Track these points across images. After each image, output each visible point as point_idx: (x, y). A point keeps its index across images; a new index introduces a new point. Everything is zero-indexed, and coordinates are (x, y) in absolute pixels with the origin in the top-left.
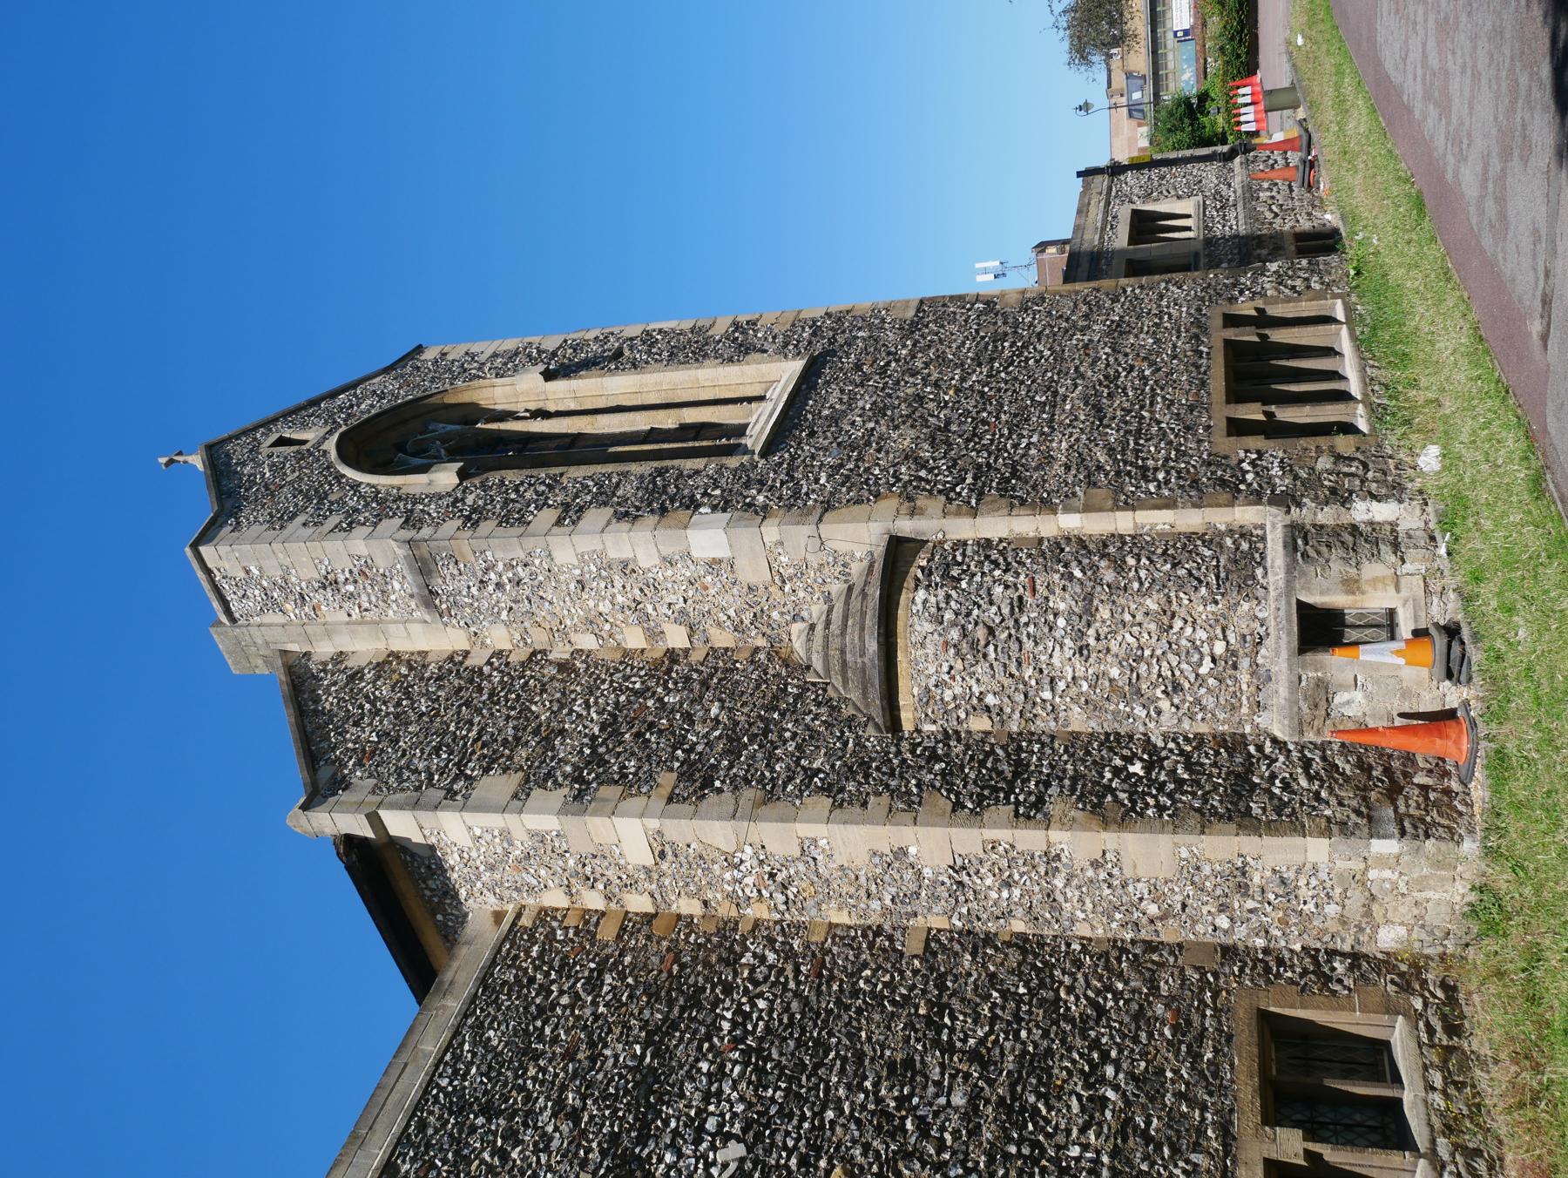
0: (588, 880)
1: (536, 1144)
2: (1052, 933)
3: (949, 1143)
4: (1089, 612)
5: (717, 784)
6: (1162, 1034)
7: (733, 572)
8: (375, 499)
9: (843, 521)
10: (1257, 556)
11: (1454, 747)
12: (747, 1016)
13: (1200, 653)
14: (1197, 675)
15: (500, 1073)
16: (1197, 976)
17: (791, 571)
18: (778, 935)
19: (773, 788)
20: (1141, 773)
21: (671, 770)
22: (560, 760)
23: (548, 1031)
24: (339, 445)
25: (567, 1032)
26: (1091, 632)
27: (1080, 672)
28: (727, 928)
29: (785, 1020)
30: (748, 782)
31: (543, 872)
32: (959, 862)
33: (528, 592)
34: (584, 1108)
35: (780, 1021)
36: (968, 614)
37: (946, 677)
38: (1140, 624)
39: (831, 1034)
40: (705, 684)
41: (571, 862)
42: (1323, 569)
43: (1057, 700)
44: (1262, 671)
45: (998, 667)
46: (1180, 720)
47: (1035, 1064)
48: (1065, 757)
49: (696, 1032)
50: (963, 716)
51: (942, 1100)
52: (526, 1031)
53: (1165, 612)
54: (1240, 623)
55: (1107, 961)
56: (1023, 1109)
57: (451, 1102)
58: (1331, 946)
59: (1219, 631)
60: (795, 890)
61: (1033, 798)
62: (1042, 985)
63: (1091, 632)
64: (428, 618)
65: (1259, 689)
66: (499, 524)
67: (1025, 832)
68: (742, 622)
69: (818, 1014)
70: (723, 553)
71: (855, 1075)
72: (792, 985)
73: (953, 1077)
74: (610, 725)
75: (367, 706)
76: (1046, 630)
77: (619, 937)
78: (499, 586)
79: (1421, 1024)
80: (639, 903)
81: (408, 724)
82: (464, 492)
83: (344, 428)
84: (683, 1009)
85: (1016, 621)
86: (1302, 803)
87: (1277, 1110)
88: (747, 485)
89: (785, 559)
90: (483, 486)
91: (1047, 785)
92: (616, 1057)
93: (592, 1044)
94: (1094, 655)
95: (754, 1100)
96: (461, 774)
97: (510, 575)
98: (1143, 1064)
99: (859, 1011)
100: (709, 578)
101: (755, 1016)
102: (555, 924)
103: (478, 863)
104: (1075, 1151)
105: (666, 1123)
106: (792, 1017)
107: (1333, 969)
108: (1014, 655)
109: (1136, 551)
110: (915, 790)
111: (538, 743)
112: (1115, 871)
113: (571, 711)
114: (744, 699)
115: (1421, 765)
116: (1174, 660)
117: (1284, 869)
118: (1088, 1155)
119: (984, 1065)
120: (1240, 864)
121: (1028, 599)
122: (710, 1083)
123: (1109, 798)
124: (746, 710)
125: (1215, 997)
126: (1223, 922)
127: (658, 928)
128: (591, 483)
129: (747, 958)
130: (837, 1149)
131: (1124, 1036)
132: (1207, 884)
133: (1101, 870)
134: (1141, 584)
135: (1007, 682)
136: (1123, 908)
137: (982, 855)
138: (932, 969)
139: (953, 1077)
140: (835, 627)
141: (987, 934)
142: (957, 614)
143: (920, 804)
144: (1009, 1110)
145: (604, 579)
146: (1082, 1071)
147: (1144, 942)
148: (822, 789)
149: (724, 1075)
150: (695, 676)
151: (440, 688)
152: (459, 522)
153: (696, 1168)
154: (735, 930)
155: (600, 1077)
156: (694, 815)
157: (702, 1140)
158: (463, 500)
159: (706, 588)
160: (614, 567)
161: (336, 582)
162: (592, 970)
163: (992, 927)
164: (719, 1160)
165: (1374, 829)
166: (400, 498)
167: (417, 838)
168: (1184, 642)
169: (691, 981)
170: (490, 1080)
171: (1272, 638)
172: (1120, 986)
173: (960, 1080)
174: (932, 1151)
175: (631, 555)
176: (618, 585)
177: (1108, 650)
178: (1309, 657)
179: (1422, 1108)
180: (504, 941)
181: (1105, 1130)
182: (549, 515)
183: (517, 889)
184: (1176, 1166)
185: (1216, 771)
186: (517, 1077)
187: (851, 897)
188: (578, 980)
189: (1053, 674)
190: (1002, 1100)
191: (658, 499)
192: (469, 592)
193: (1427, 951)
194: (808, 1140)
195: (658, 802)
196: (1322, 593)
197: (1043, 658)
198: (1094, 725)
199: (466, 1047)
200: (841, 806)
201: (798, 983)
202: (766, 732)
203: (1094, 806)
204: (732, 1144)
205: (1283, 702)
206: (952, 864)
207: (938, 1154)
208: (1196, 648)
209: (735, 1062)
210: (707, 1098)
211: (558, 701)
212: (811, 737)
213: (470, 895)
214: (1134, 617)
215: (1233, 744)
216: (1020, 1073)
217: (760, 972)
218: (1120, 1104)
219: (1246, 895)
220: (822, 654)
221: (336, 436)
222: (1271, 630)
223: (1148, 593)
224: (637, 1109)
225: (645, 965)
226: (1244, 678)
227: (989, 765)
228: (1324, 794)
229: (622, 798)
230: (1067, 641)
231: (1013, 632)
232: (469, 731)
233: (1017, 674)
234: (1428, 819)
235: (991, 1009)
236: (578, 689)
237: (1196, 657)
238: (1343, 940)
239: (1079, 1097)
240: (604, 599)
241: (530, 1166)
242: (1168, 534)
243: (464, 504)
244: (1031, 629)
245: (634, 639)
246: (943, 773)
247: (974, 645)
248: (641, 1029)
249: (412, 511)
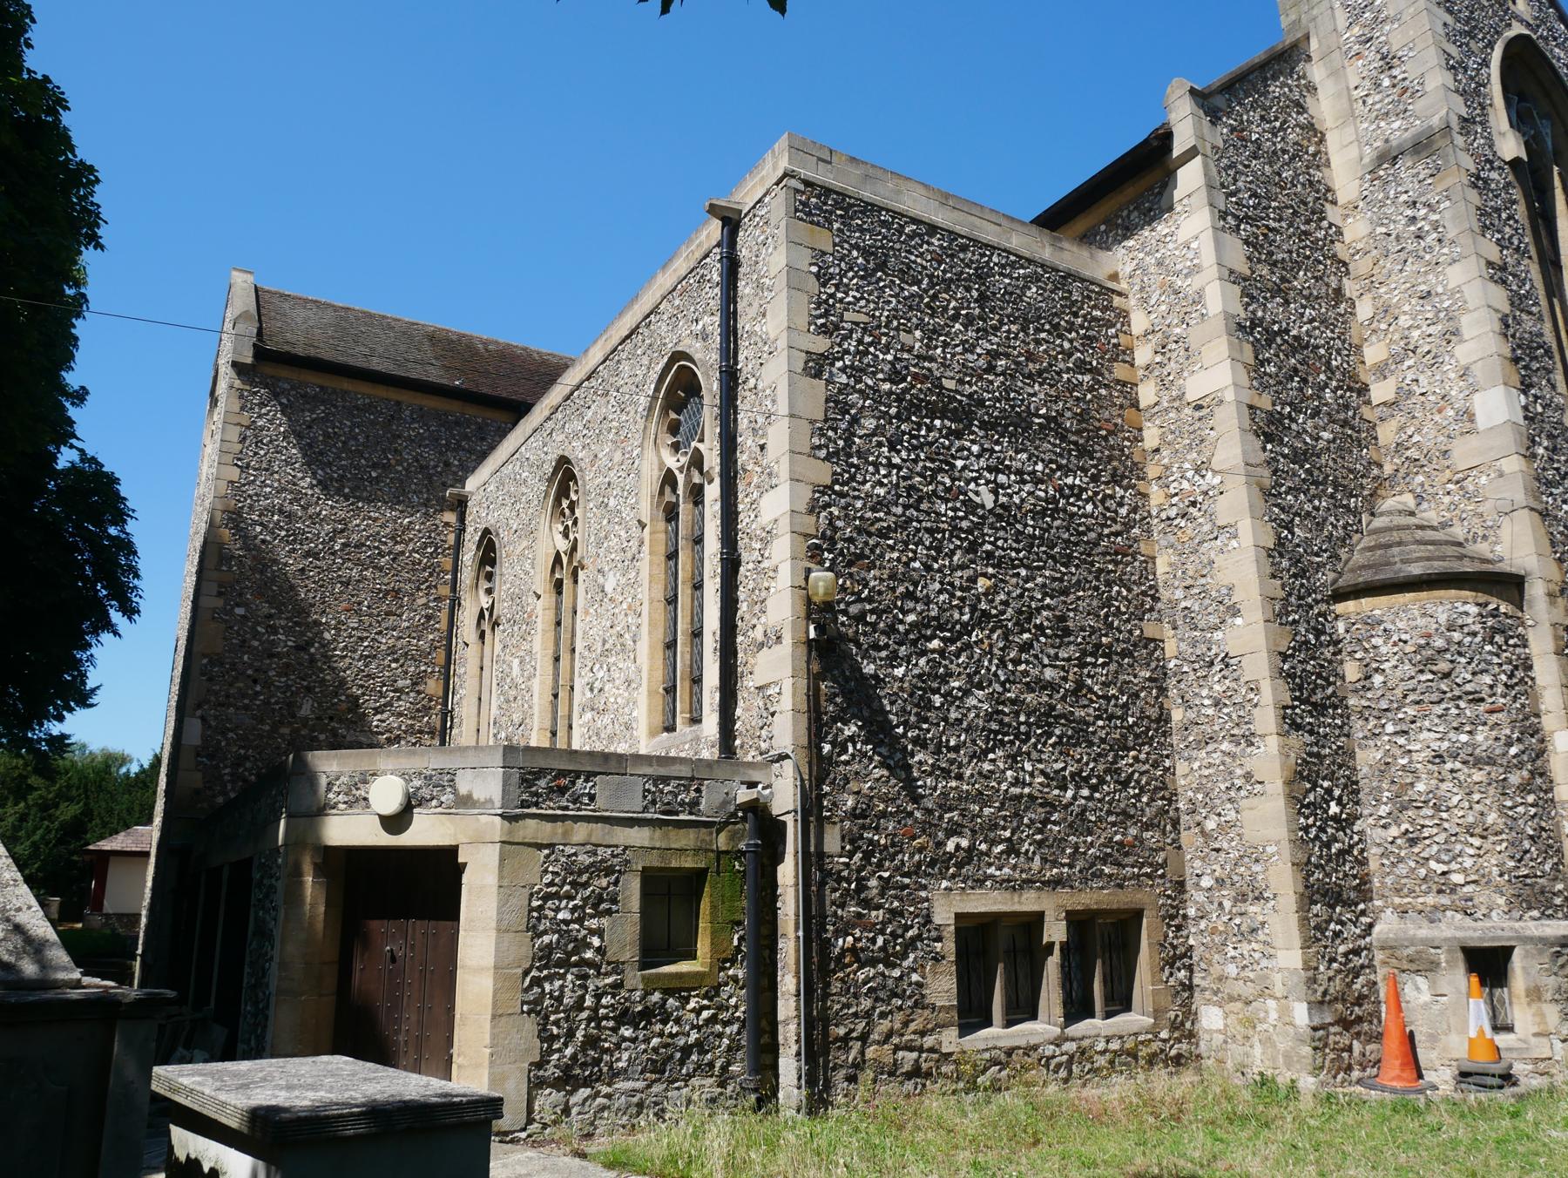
0: (1162, 349)
1: (967, 341)
2: (1175, 743)
3: (1019, 668)
4: (1478, 763)
5: (1269, 446)
6: (1116, 833)
7: (1462, 434)
8: (1479, 85)
9: (1534, 531)
10: (1550, 912)
11: (1393, 1073)
12: (1079, 497)
13: (1450, 862)
14: (1427, 859)
15: (1008, 302)
16: (1160, 861)
17: (1471, 488)
18: (1139, 516)
19: (1274, 495)
20: (1331, 812)
21: (1274, 405)
22: (1265, 305)
23: (1043, 335)
24: (1519, 37)
25: (1045, 351)
26: (1458, 765)
27: (1415, 756)
28: (1137, 470)
29: (1081, 529)
30: (1275, 472)
32: (1232, 661)
33: (1410, 247)
34: (997, 375)
35: (1079, 525)
36: (1460, 654)
37: (1395, 638)
38: (1471, 808)
39: (1077, 567)
40: (1345, 423)
41: (1178, 330)
42: (1547, 970)
43: (1386, 738)
44: (1439, 915)
45: (1411, 684)
46: (1379, 845)
47: (1080, 736)
48: (1334, 747)
49: (1061, 455)
50: (1358, 656)
51: (1046, 661)
52: (1040, 317)
53: (1486, 830)
54: (1482, 896)
55: (1161, 789)
56: (1049, 725)
57: (983, 268)
58: (1196, 968)
59: (1474, 877)
60: (1182, 524)
61: (1299, 721)
62: (1137, 736)
63: (1458, 765)
64: (1366, 160)
65: (1420, 912)
66: (1478, 209)
67: (1273, 714)
68: (1407, 449)
69: (1089, 555)
70: (1482, 422)
71: (1053, 590)
72: (1106, 531)
73: (1063, 668)
74: (1299, 344)
75: (1278, 124)
76: (1455, 724)
77: (1118, 382)
78: (1413, 220)
79: (1150, 1036)
80: (1147, 394)
81: (1271, 164)
82: (1500, 168)
83: (1535, 37)
84: (1075, 443)
85: (1460, 698)
86: (1326, 947)
87: (1078, 922)
88: (1550, 436)
89: (1484, 480)
90: (1508, 184)
91: (1311, 733)
92: (1034, 395)
93: (1040, 372)
94: (1435, 768)
95: (1023, 510)
96: (1240, 220)
97: (1427, 228)
98: (1093, 819)
99: (1096, 588)
100: (1451, 413)
101: (1080, 503)
102: (1119, 326)
103: (1163, 251)
104: (1028, 766)
105: (997, 443)
106: (1084, 533)
107: (1179, 970)
108: (1426, 698)
109: (1541, 803)
110: (1290, 619)
111: (1275, 283)
112: (1243, 793)
113: (1304, 307)
114: (1339, 460)
115: (1368, 1048)
116: (1441, 838)
117: (1267, 931)
118: (1027, 777)
119: (1075, 692)
120: (1266, 895)
121: (1482, 707)
122: (1029, 474)
123: (1308, 786)
124: (1331, 463)
125: (1147, 875)
126: (1206, 882)
127: (1129, 413)
128: (1527, 287)
129: (1119, 492)
130: (1002, 581)
131: (1110, 803)
132: (1242, 869)
133: (1243, 780)
134: (1511, 808)
135: (1398, 692)
136: (1208, 800)
137: (1243, 680)
138: (1135, 645)
139: (1063, 668)
140: (1419, 534)
141: (1166, 689)
142: (1459, 643)
143: (1281, 624)
144: (1048, 715)
145: (1436, 315)
146: (1082, 771)
147: (1179, 818)
148: (1279, 538)
149: (1036, 484)
150: (1350, 413)
151: (1303, 185)
152: (1473, 170)
153: (972, 471)
154: (1139, 478)
155: (1019, 384)
156: (1243, 430)
157: (990, 473)
158: (1492, 168)
159: (1440, 411)
160: (1451, 323)
161: (1390, 68)
162: (1090, 363)
163: (1173, 693)
164: (980, 488)
165: (1318, 1004)
166: (1483, 108)
167: (1178, 194)
168: (1458, 847)
169: (1097, 448)
170: (1003, 295)
171: (1474, 924)
172: (1145, 799)
173: (1062, 674)
174: (1012, 655)
175: (1466, 337)
176: (1431, 330)
177: (1442, 781)
178: (1460, 955)
179: (1093, 1033)
180: (1100, 286)
181: (1046, 790)
182: (1493, 253)
183: (1142, 289)
184: (1030, 844)
185: (1341, 876)
186: (1008, 317)
187: (1183, 573)
188: (1082, 353)
189: (1412, 733)
190: (1053, 708)
191: (1524, 353)
192: (1401, 193)
193: (1202, 1044)
194: (1004, 557)
195: (1248, 396)
196: (1524, 968)
197: (1427, 723)
198: (1364, 771)
199: (1022, 271)
200: (1269, 556)
201: (1108, 536)
202: (1316, 483)
203: (1300, 773)
204: (992, 497)
205: (1411, 933)
206: (1231, 655)
207: (1011, 660)
208: (1454, 858)
209: (1046, 492)
210: (1019, 472)
211: (1311, 294)
212: (1318, 524)
213: (1130, 249)
214: (1478, 802)
215: (1364, 891)
216: (1074, 721)
217: (1110, 503)
218: (1064, 802)
219: (1236, 901)
220: (1391, 525)
221: (1526, 32)
222: (1480, 924)
223: (1502, 814)
224: (1003, 418)
225: (1101, 407)
226: (1431, 899)
227: (1319, 681)
228: (1335, 965)
229: (1246, 365)
230: (1446, 744)
231: (1449, 695)
232: (1274, 219)
233: (1407, 701)
234: (1327, 1051)
235: (1113, 695)
236: (1323, 310)
237: (1446, 858)
238: (1203, 978)
239: (1064, 769)
241: (952, 339)
242: (1559, 832)
243: (1489, 171)
244: (1454, 711)
245: (1374, 353)
246: (1307, 642)
247: (1431, 660)
248: (1057, 411)
249: (1474, 123)
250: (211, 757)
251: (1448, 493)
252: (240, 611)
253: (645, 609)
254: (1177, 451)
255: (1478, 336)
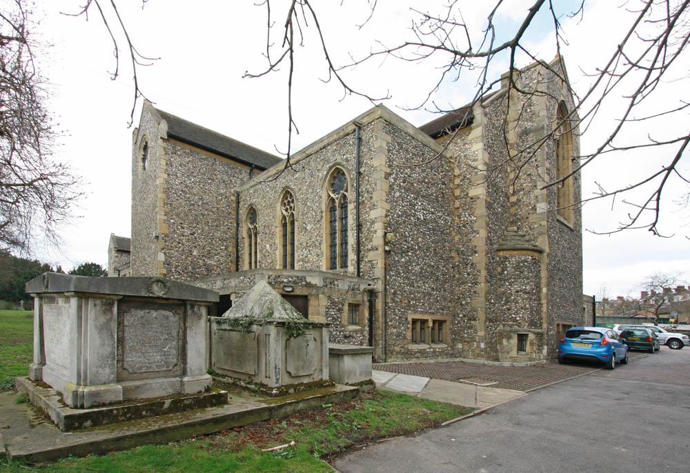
4: (526, 293)
31: (465, 169)
70: (538, 211)
219: (468, 320)
226: (511, 323)
250: (168, 265)
252: (172, 221)
253: (324, 236)
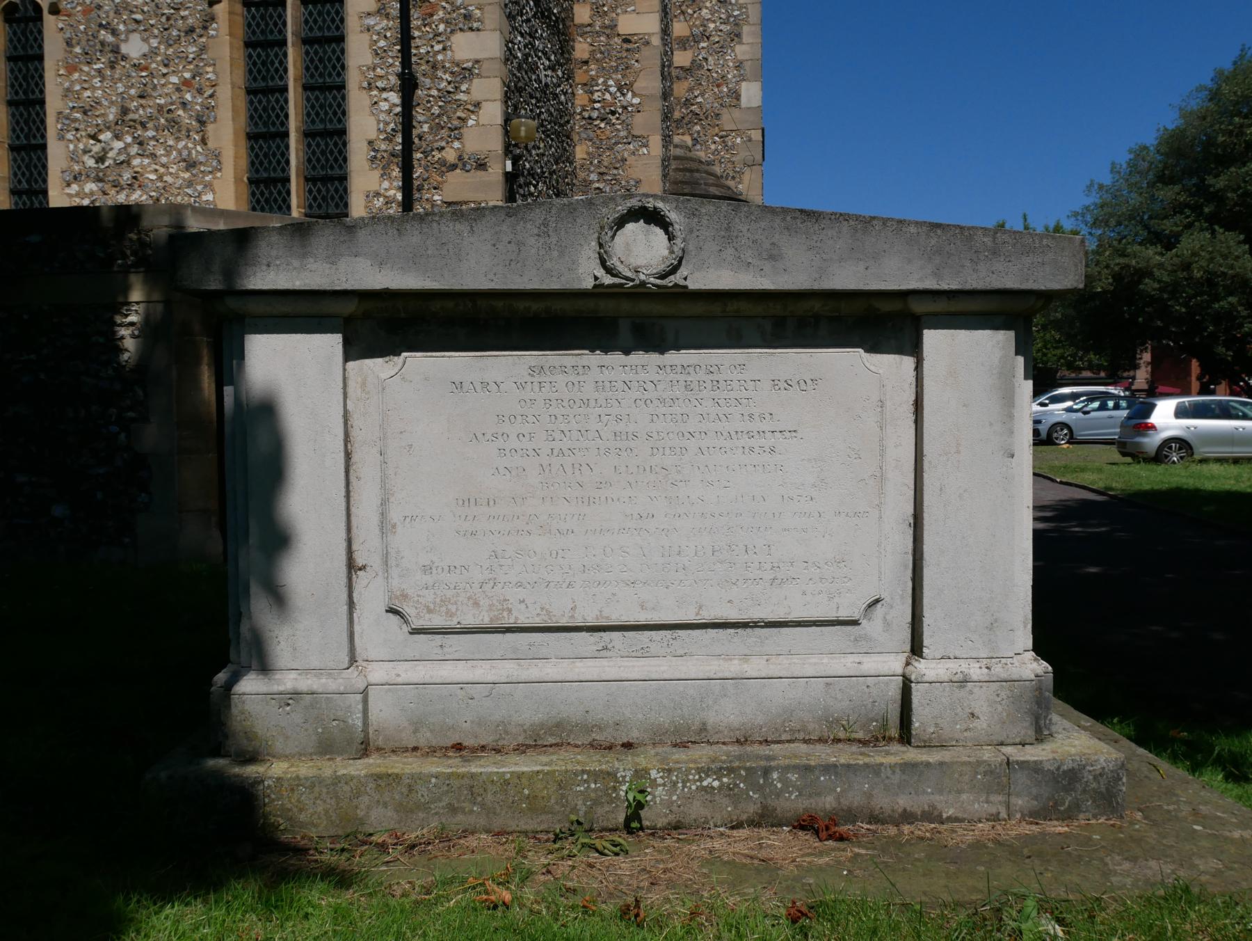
17: (730, 144)
70: (744, 102)
89: (739, 140)
175: (744, 41)
176: (722, 27)
187: (599, 162)
240: (711, 14)
251: (715, 143)
254: (604, 68)
255: (752, 43)
